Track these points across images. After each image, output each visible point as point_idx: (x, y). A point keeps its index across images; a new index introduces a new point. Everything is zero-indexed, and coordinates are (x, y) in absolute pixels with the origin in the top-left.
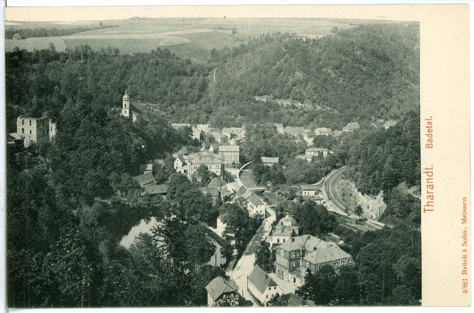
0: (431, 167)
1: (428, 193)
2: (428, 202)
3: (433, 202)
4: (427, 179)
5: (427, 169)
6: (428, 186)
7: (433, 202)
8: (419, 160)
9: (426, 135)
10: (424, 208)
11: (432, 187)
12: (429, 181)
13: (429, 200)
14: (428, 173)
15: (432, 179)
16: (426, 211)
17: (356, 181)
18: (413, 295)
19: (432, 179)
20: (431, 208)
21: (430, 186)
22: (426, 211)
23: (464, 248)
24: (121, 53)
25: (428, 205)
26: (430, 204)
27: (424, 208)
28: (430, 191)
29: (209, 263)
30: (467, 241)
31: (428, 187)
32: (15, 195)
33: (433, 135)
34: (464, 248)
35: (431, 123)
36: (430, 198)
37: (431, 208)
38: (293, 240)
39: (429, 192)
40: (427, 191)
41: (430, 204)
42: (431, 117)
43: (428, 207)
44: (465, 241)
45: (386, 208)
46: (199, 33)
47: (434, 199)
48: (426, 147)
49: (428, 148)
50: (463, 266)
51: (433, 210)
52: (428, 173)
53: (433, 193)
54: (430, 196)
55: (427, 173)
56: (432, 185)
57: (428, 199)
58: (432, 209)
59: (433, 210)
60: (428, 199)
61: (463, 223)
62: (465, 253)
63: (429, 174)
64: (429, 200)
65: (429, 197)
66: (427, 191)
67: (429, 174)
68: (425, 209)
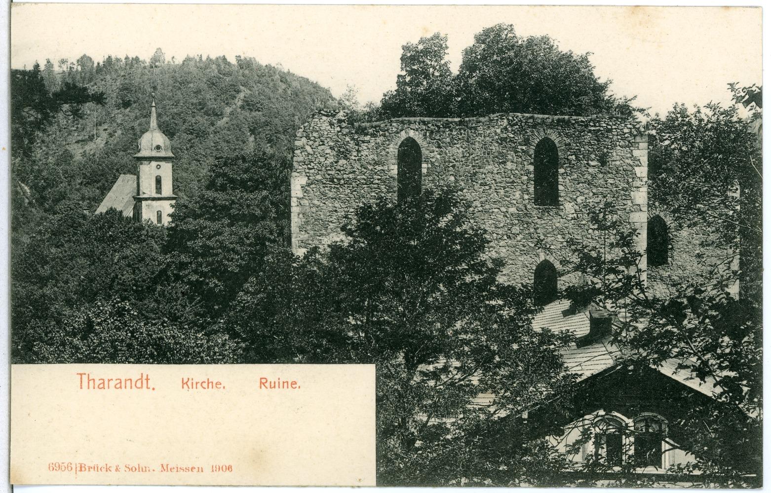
1: (109, 380)
2: (94, 380)
4: (131, 380)
5: (147, 379)
11: (119, 385)
12: (128, 383)
13: (97, 382)
15: (131, 388)
17: (316, 275)
18: (24, 350)
19: (131, 388)
21: (104, 383)
23: (122, 468)
25: (89, 380)
26: (91, 382)
28: (112, 384)
30: (52, 461)
31: (102, 381)
35: (118, 386)
38: (695, 106)
39: (111, 382)
41: (91, 382)
42: (154, 389)
44: (134, 469)
48: (261, 379)
49: (261, 382)
50: (93, 466)
51: (81, 388)
55: (141, 379)
59: (81, 388)
61: (162, 465)
62: (113, 469)
64: (97, 382)
65: (102, 381)
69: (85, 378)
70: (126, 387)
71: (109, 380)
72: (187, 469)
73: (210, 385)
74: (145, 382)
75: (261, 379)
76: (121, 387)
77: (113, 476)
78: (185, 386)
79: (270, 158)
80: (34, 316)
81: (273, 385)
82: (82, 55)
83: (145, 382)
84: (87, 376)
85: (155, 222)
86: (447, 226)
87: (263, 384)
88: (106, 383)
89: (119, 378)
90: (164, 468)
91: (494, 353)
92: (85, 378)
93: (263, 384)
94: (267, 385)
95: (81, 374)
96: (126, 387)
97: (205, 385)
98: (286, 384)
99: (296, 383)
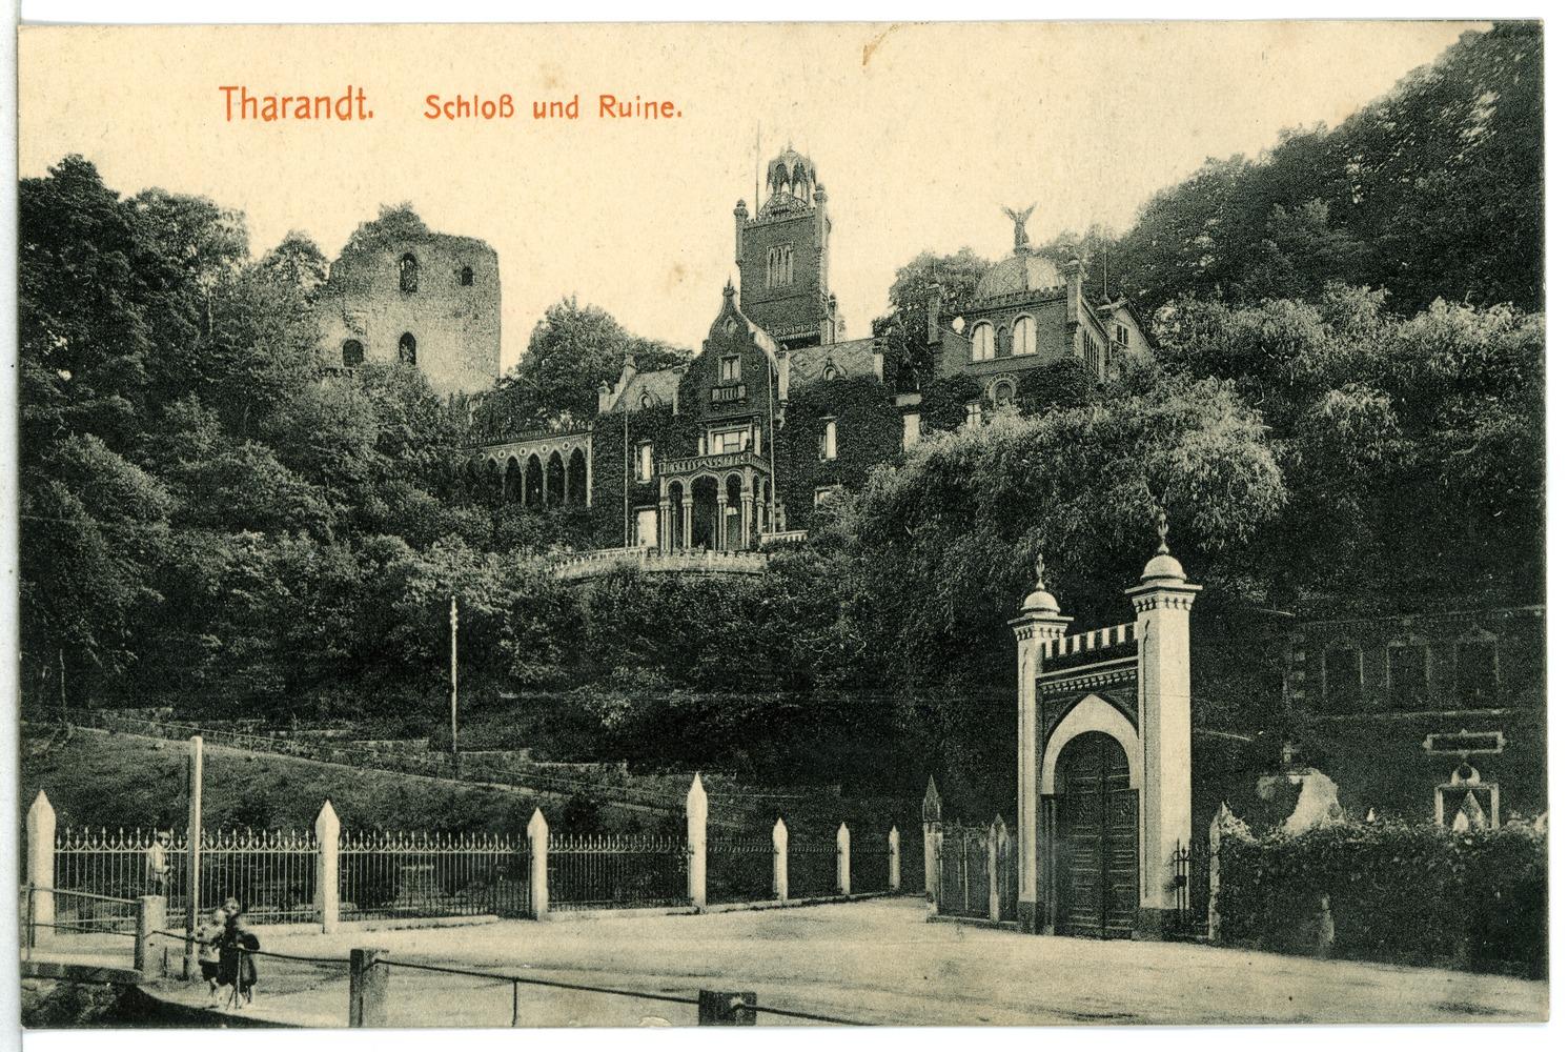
0: (366, 111)
2: (254, 100)
3: (255, 116)
5: (361, 98)
6: (307, 99)
7: (255, 116)
9: (576, 97)
10: (236, 88)
11: (461, 925)
12: (323, 105)
13: (261, 105)
14: (346, 102)
16: (225, 92)
19: (244, 116)
20: (236, 110)
22: (225, 92)
25: (245, 101)
26: (250, 105)
27: (236, 88)
28: (292, 107)
31: (270, 103)
32: (644, 405)
34: (590, 105)
36: (268, 108)
37: (236, 110)
40: (291, 99)
41: (250, 105)
42: (371, 114)
43: (240, 100)
46: (550, 887)
48: (602, 97)
51: (229, 119)
52: (346, 102)
53: (284, 115)
54: (307, 106)
56: (307, 115)
57: (266, 99)
58: (287, 113)
59: (229, 119)
60: (266, 99)
63: (345, 104)
64: (261, 105)
65: (270, 103)
66: (291, 99)
67: (345, 104)
68: (233, 93)
69: (236, 96)
70: (317, 116)
71: (285, 101)
72: (305, 109)
73: (463, 109)
74: (355, 104)
75: (602, 97)
77: (620, 981)
78: (605, 112)
79: (276, 314)
80: (1454, 863)
81: (625, 111)
83: (355, 104)
84: (240, 92)
85: (350, 305)
87: (608, 107)
89: (272, 95)
90: (607, 104)
92: (236, 96)
93: (608, 107)
94: (615, 109)
95: (229, 89)
96: (317, 116)
97: (453, 110)
98: (323, 105)
99: (672, 107)
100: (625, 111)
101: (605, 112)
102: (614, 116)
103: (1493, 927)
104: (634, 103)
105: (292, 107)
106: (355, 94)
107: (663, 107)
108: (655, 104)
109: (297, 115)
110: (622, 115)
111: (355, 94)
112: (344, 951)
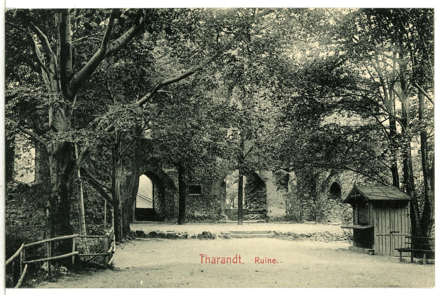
1: (218, 259)
2: (209, 258)
4: (230, 258)
5: (240, 258)
8: (11, 104)
12: (229, 260)
13: (211, 260)
19: (206, 263)
21: (215, 260)
24: (337, 225)
25: (206, 258)
26: (208, 260)
28: (220, 260)
29: (379, 82)
33: (235, 264)
39: (219, 259)
40: (220, 258)
41: (208, 260)
45: (228, 176)
47: (212, 264)
49: (256, 259)
54: (215, 260)
56: (224, 262)
64: (211, 260)
65: (214, 259)
66: (220, 258)
71: (218, 259)
74: (238, 259)
76: (215, 262)
78: (257, 262)
81: (262, 262)
82: (436, 284)
83: (238, 259)
86: (56, 159)
87: (257, 261)
88: (226, 260)
91: (16, 36)
93: (257, 261)
98: (229, 260)
99: (275, 260)
100: (262, 262)
101: (257, 262)
102: (259, 263)
103: (9, 284)
104: (265, 259)
105: (220, 260)
106: (238, 256)
107: (273, 261)
108: (270, 260)
109: (222, 263)
110: (261, 263)
111: (238, 256)
112: (201, 233)
